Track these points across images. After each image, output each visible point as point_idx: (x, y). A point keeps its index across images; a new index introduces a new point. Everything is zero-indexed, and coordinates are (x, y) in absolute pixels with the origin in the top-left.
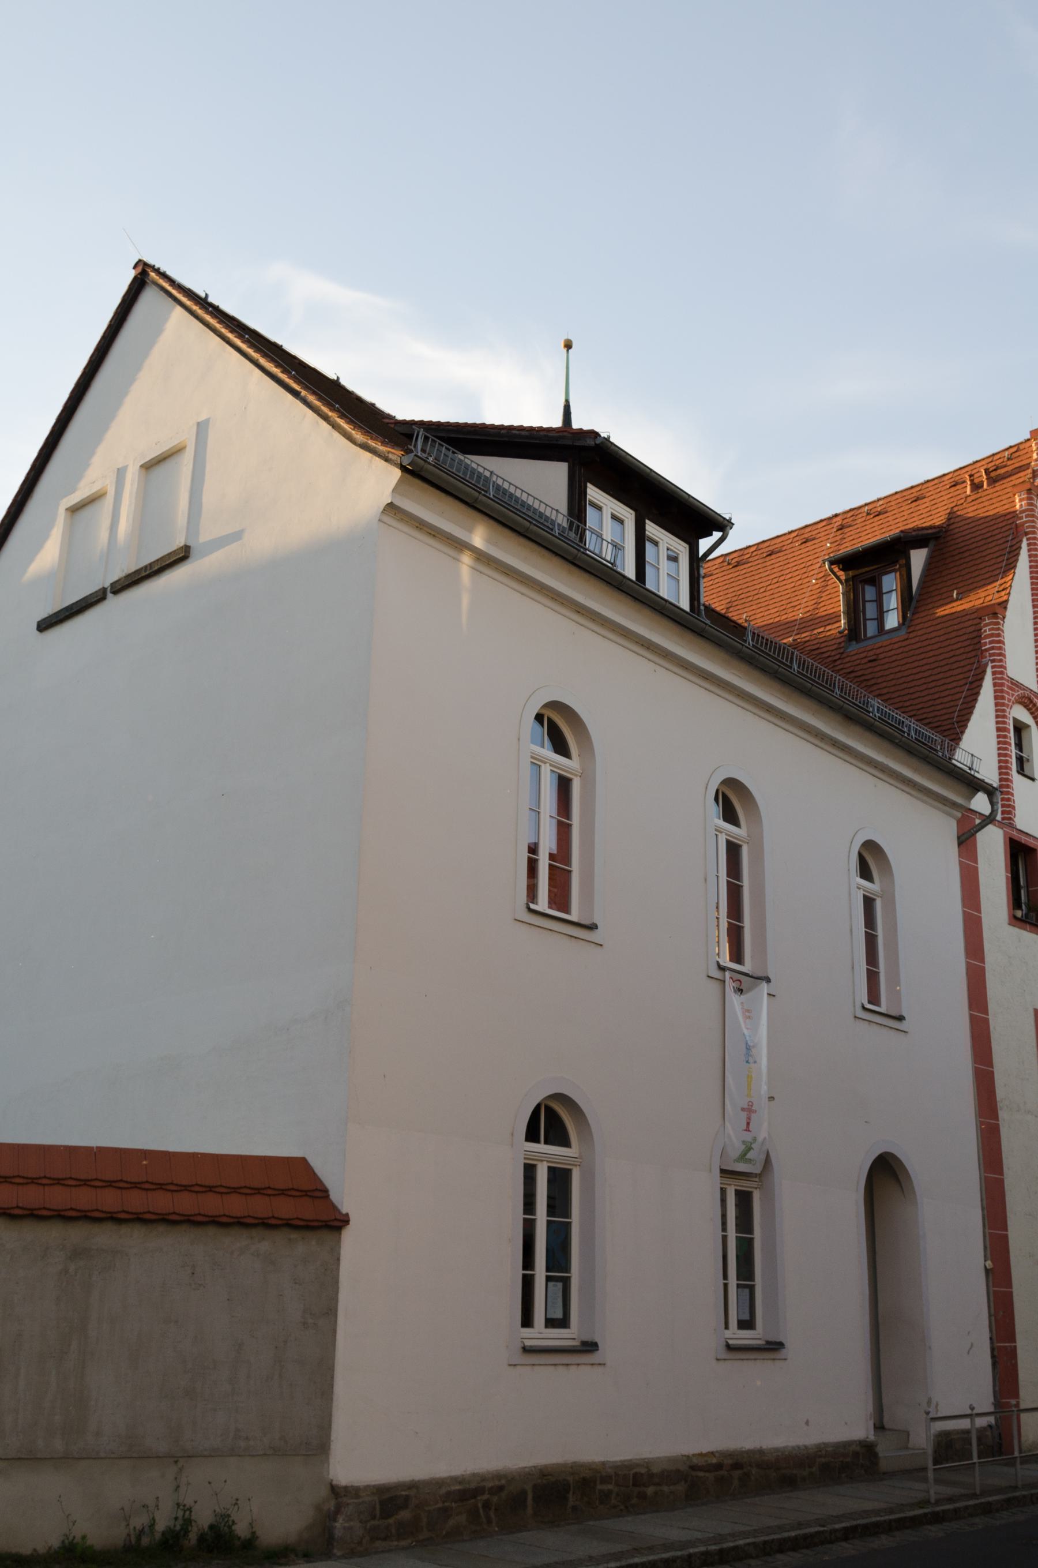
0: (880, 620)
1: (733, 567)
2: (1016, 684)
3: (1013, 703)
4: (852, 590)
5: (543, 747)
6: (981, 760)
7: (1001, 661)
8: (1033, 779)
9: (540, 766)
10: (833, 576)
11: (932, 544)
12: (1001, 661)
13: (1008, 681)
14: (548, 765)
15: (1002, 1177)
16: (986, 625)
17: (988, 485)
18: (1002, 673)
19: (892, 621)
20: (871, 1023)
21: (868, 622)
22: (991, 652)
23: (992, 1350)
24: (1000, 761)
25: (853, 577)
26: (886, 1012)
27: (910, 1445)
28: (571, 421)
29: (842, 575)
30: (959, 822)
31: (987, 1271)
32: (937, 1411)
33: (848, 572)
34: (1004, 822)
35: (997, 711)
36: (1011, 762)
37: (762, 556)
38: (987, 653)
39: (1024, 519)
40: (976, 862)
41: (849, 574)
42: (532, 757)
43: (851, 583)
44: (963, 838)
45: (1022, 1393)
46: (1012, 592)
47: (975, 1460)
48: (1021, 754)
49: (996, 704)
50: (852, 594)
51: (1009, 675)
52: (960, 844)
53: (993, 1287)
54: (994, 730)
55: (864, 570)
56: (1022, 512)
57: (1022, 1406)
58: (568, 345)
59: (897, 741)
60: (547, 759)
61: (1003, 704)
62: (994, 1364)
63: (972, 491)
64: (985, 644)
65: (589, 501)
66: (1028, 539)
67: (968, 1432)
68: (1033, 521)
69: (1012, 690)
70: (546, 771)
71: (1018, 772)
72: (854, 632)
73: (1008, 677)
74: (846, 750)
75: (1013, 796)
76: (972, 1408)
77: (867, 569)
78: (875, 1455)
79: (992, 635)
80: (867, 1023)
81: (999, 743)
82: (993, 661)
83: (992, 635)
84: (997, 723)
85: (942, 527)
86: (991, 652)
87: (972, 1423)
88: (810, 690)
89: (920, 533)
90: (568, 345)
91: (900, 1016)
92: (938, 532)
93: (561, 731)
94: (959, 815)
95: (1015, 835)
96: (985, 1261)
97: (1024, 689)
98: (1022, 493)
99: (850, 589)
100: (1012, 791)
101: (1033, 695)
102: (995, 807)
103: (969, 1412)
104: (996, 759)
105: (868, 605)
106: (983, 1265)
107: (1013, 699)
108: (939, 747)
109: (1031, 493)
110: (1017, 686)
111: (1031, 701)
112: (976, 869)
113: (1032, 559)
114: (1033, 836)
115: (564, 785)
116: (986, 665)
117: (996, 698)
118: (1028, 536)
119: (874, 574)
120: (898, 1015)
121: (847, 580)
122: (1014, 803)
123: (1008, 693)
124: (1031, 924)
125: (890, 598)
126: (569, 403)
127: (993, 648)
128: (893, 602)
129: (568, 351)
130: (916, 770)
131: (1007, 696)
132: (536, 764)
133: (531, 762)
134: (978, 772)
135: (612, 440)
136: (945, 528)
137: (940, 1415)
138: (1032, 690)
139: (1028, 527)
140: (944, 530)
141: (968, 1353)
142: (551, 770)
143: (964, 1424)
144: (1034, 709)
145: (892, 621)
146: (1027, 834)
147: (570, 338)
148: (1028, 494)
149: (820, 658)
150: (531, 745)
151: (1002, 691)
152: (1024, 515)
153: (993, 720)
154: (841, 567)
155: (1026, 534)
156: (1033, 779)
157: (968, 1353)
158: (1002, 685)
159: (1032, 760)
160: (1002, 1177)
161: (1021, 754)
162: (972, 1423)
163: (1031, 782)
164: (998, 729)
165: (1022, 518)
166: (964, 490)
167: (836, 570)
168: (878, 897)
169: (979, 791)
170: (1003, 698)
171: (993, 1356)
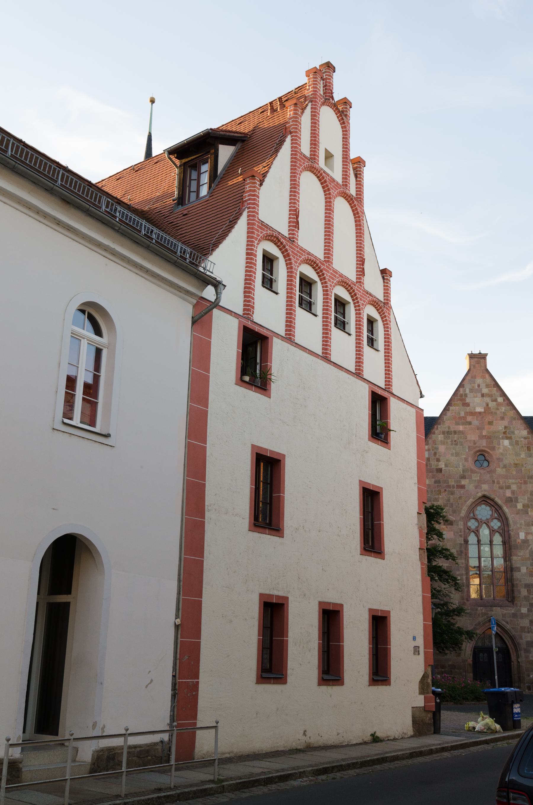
0: (198, 192)
1: (135, 172)
2: (264, 226)
3: (336, 285)
4: (182, 172)
5: (84, 329)
6: (214, 264)
7: (254, 208)
8: (277, 293)
9: (80, 340)
10: (169, 161)
11: (239, 145)
12: (254, 208)
13: (259, 222)
14: (86, 339)
15: (203, 559)
16: (248, 184)
17: (280, 109)
18: (254, 216)
19: (204, 191)
20: (71, 435)
21: (191, 194)
22: (248, 202)
23: (174, 685)
24: (246, 275)
25: (184, 163)
26: (99, 432)
27: (77, 759)
28: (151, 144)
29: (178, 162)
30: (195, 306)
31: (177, 627)
32: (104, 732)
33: (181, 160)
34: (244, 316)
35: (248, 241)
36: (295, 298)
37: (152, 164)
38: (246, 203)
39: (291, 124)
40: (210, 338)
41: (182, 162)
42: (72, 333)
43: (183, 167)
44: (196, 318)
45: (199, 716)
46: (272, 166)
47: (124, 769)
48: (310, 300)
49: (248, 237)
50: (182, 175)
51: (260, 218)
52: (194, 322)
53: (181, 638)
54: (245, 254)
55: (190, 159)
56: (290, 119)
57: (198, 726)
58: (152, 101)
59: (117, 228)
60: (84, 336)
61: (252, 237)
62: (174, 696)
63: (270, 113)
64: (245, 197)
65: (301, 279)
66: (292, 136)
67: (121, 748)
68: (296, 125)
69: (261, 229)
70: (84, 343)
71: (335, 326)
72: (181, 200)
73: (260, 220)
74: (71, 230)
75: (363, 357)
76: (127, 730)
77: (193, 157)
78: (19, 770)
79: (250, 191)
80: (68, 435)
81: (247, 263)
82: (249, 208)
83: (250, 191)
84: (247, 249)
85: (247, 134)
86: (248, 202)
87: (126, 741)
88: (52, 189)
89: (228, 134)
90: (152, 101)
91: (108, 434)
92: (244, 137)
93: (94, 317)
94: (195, 302)
95: (249, 325)
96: (176, 619)
97: (273, 231)
98: (291, 106)
99: (181, 172)
100: (253, 296)
101: (281, 236)
102: (219, 295)
103: (124, 732)
104: (243, 273)
105: (192, 182)
106: (174, 621)
107: (335, 282)
108: (188, 256)
109: (297, 107)
110: (267, 228)
111: (279, 241)
112: (210, 343)
113: (293, 149)
114: (266, 328)
115: (98, 352)
116: (244, 210)
117: (248, 233)
118: (292, 135)
119: (196, 161)
120: (107, 433)
121: (180, 166)
122: (330, 343)
123: (258, 231)
124: (256, 386)
125: (205, 176)
126: (151, 134)
127: (249, 199)
128: (205, 178)
129: (152, 104)
130: (145, 258)
131: (363, 299)
132: (76, 337)
133: (71, 336)
134: (212, 273)
135: (473, 353)
136: (249, 135)
137: (105, 734)
138: (280, 233)
139: (293, 128)
140: (249, 136)
141: (147, 687)
142: (88, 343)
143: (118, 742)
144: (377, 306)
145: (204, 191)
146: (261, 325)
147: (154, 97)
148: (294, 107)
149: (172, 228)
150: (72, 326)
151: (253, 228)
152: (291, 120)
153: (245, 247)
154: (176, 156)
155: (291, 133)
156: (377, 350)
157: (147, 687)
158: (254, 224)
159: (350, 323)
160: (203, 559)
161: (310, 300)
162: (126, 741)
163: (275, 294)
164: (247, 254)
165: (289, 123)
166: (267, 114)
167: (174, 159)
168: (105, 347)
169: (209, 284)
170: (253, 233)
171: (174, 688)
